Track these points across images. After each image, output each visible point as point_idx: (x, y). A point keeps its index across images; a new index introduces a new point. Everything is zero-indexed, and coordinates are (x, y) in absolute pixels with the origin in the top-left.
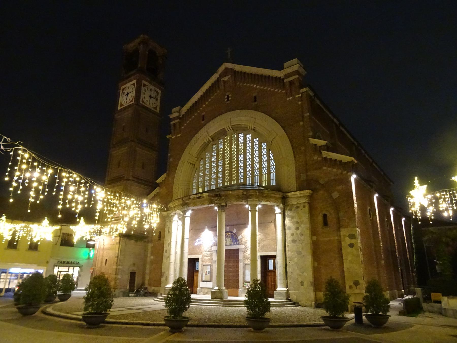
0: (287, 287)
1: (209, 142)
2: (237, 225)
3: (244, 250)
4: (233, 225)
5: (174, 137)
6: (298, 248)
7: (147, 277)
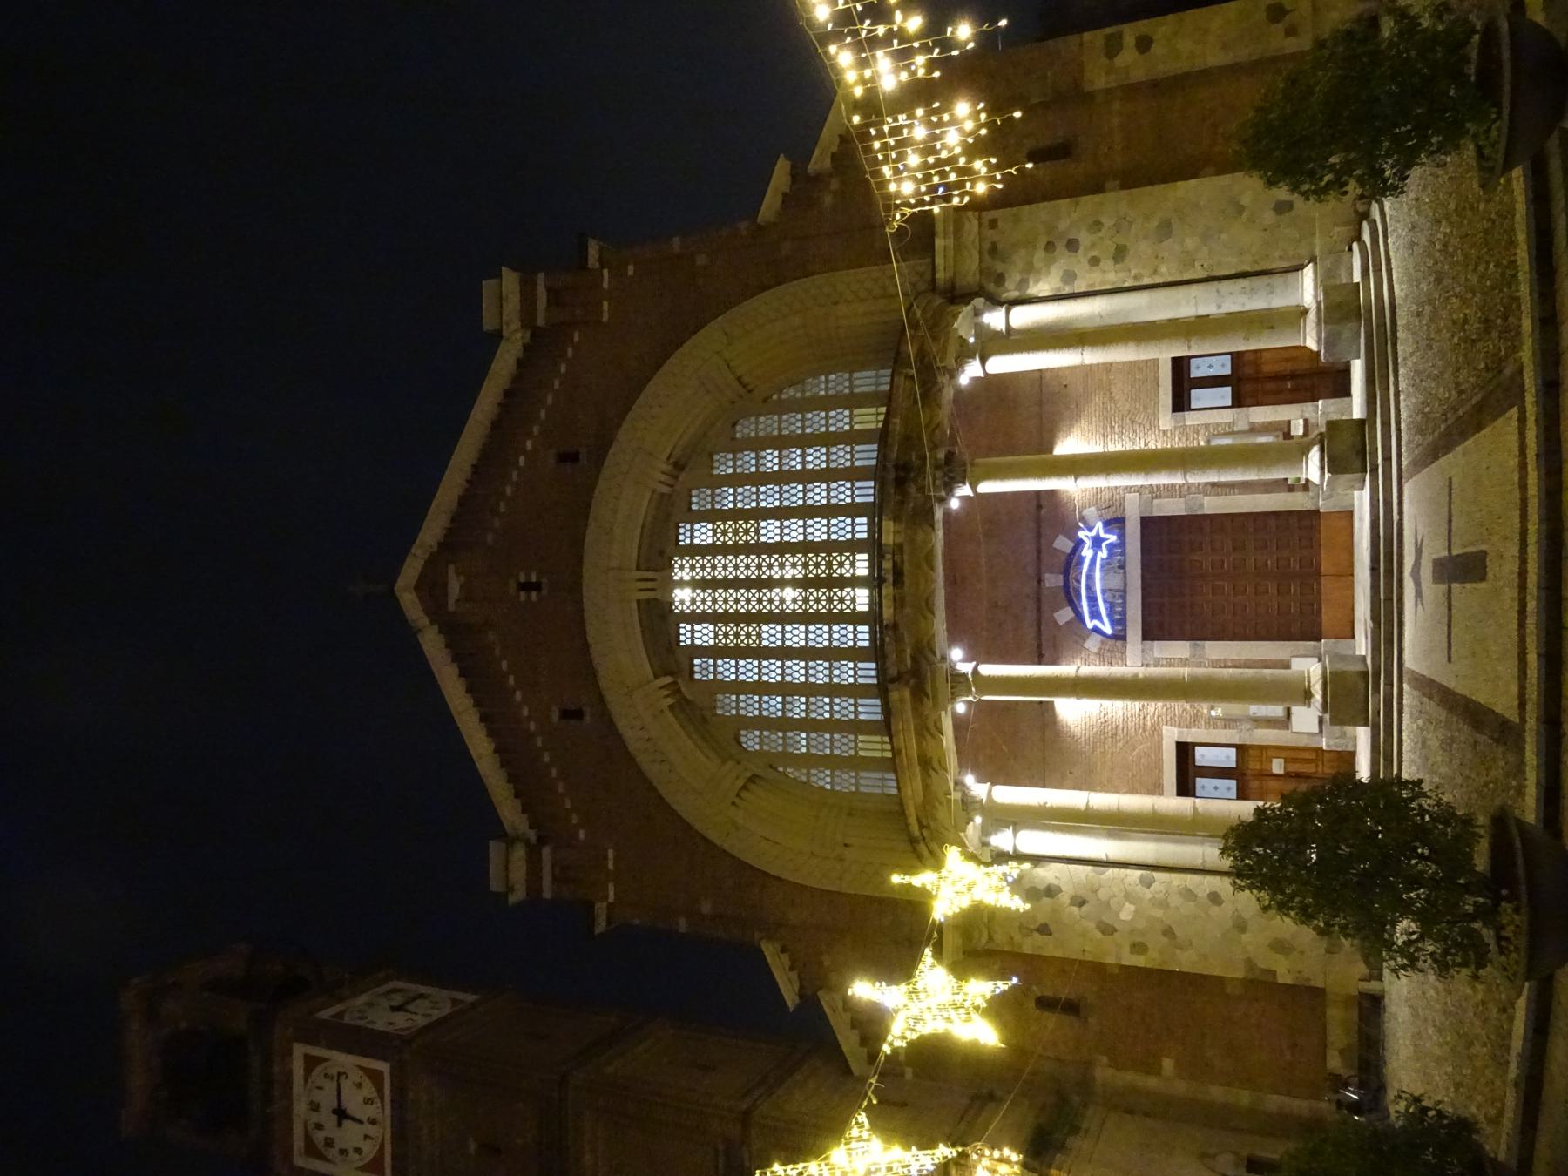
0: (1301, 267)
1: (675, 690)
2: (1039, 535)
3: (1147, 495)
4: (1039, 552)
5: (611, 887)
6: (1146, 237)
7: (1274, 1102)
